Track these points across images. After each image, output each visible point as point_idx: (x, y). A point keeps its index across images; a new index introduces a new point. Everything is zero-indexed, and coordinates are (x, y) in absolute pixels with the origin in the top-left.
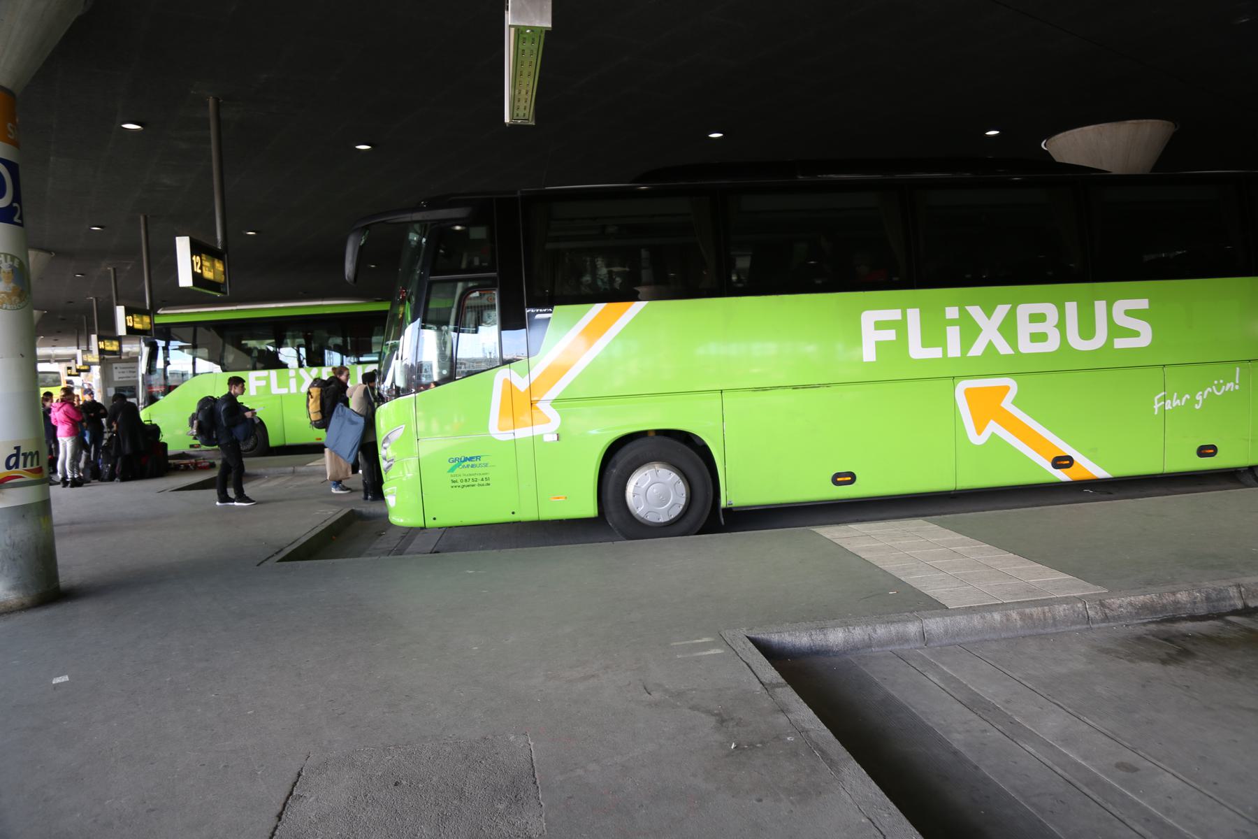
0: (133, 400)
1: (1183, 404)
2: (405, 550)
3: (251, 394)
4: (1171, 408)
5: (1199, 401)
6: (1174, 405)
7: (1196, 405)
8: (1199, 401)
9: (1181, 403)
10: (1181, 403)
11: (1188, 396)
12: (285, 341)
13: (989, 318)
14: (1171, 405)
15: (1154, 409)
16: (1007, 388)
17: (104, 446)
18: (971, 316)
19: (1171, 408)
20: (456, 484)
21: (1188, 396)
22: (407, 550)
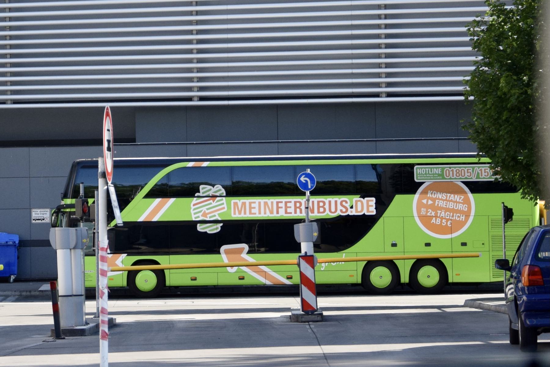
7: (322, 268)
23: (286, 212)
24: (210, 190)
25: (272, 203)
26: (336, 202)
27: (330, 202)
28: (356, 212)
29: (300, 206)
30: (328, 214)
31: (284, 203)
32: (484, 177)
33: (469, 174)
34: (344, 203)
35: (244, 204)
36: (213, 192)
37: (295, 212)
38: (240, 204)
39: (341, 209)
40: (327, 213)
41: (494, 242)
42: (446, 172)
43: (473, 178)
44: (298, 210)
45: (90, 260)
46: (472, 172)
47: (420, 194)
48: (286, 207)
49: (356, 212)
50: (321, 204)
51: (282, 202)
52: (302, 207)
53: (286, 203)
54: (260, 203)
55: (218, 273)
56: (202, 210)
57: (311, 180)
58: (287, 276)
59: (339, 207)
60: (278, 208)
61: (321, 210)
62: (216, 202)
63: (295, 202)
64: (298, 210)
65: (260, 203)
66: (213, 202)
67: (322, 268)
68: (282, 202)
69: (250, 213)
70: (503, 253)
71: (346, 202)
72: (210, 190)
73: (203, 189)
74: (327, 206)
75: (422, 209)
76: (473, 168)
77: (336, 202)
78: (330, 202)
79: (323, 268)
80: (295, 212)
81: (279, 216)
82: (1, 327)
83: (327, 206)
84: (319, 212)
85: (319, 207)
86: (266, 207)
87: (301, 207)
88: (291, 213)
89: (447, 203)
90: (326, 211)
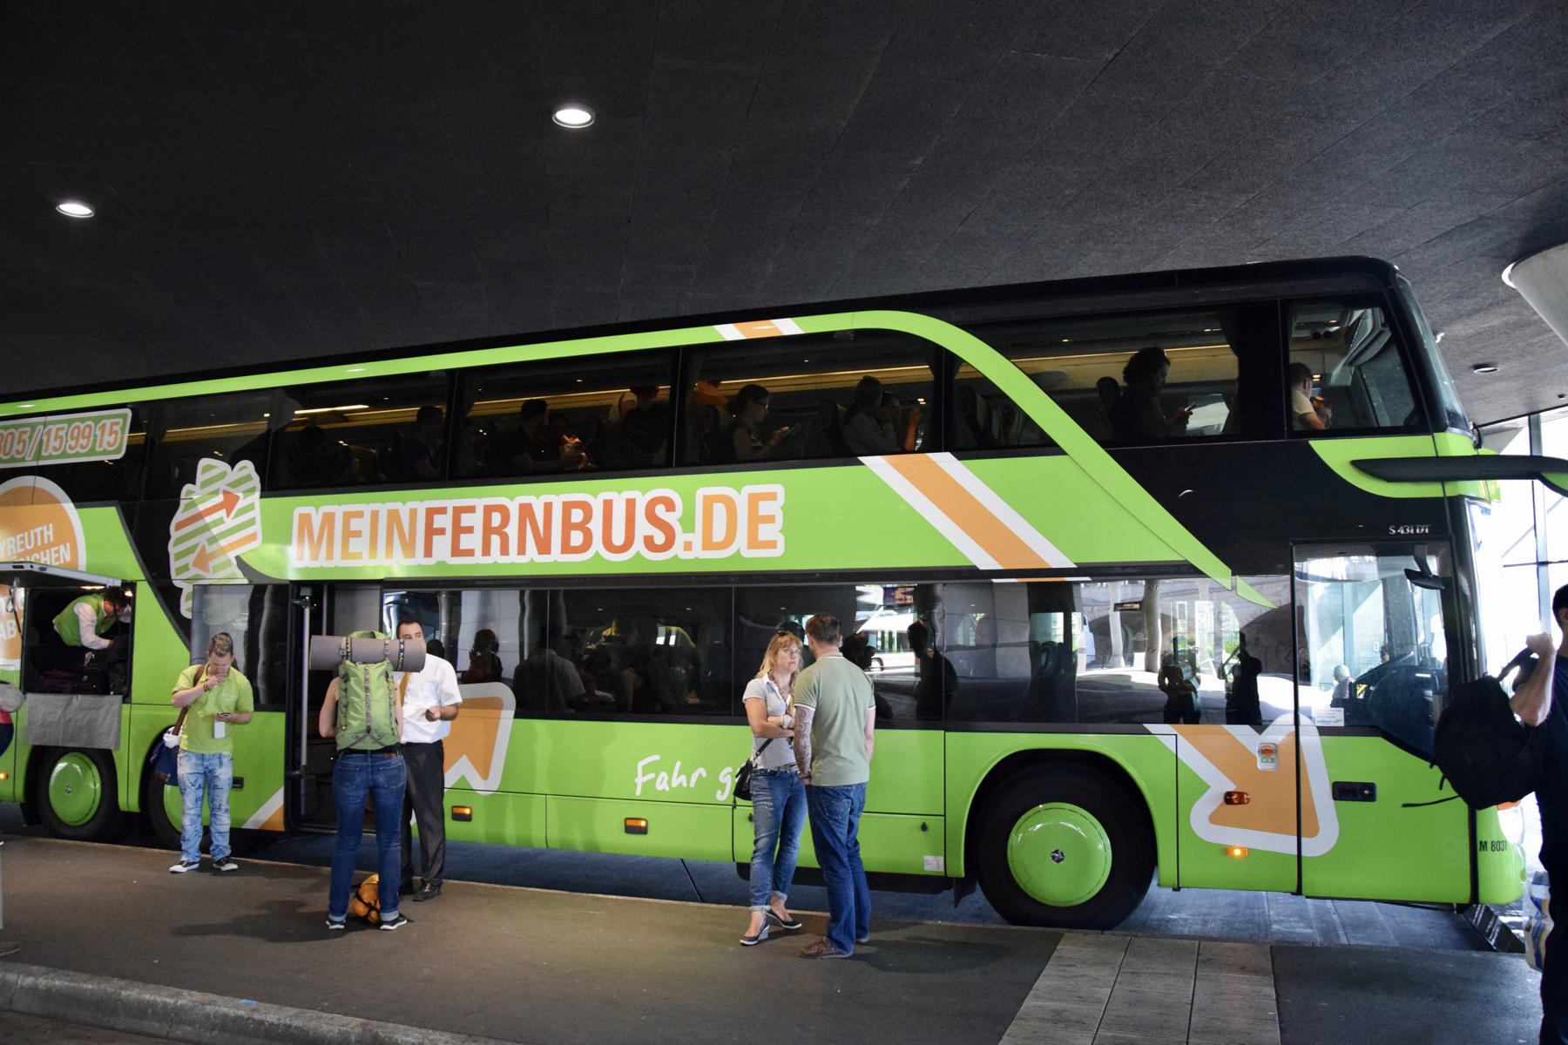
0: (1536, 317)
1: (692, 785)
2: (1015, 1015)
3: (1296, 429)
4: (667, 789)
5: (725, 784)
6: (674, 785)
7: (719, 792)
8: (725, 784)
9: (688, 782)
10: (688, 782)
11: (702, 771)
12: (45, 988)
13: (463, 777)
14: (669, 783)
15: (636, 784)
16: (485, 776)
17: (698, 697)
18: (507, 756)
19: (667, 789)
20: (224, 795)
21: (702, 771)
22: (1018, 1014)
23: (456, 551)
24: (224, 474)
25: (413, 512)
26: (631, 504)
27: (608, 505)
28: (705, 548)
29: (500, 525)
30: (600, 556)
31: (450, 512)
32: (105, 450)
33: (20, 447)
34: (660, 510)
35: (329, 519)
36: (228, 485)
37: (486, 551)
38: (317, 522)
39: (648, 533)
40: (638, 553)
42: (73, 429)
43: (27, 458)
44: (495, 540)
45: (126, 707)
46: (27, 441)
47: (59, 503)
48: (458, 530)
49: (705, 548)
50: (577, 516)
51: (471, 509)
52: (509, 526)
53: (458, 511)
54: (375, 514)
55: (943, 818)
56: (198, 544)
57: (115, 450)
58: (626, 819)
59: (643, 528)
60: (431, 532)
61: (577, 538)
62: (236, 516)
63: (489, 510)
64: (495, 540)
65: (375, 514)
66: (228, 515)
67: (719, 792)
68: (471, 509)
69: (754, 543)
70: (133, 712)
71: (670, 506)
72: (224, 474)
73: (208, 468)
74: (596, 525)
75: (660, 641)
76: (33, 427)
77: (631, 504)
78: (608, 505)
79: (722, 794)
80: (486, 551)
81: (433, 563)
82: (1563, 242)
83: (596, 525)
84: (567, 548)
85: (568, 526)
86: (304, 529)
87: (505, 527)
88: (470, 553)
89: (22, 539)
90: (593, 546)
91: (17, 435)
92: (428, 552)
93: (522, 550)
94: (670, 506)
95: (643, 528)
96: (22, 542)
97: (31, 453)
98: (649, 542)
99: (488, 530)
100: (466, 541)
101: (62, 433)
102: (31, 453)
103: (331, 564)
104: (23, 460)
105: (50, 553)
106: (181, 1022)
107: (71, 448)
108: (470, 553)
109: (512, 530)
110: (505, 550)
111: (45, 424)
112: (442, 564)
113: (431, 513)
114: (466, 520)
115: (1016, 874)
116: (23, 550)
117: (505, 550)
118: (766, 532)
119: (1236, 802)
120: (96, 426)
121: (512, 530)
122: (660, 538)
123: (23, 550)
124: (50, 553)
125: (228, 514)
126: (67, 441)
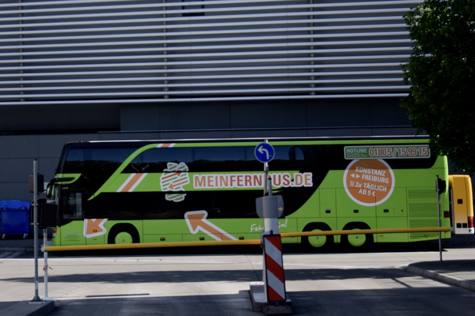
0: (32, 224)
23: (239, 185)
26: (280, 176)
34: (286, 177)
35: (204, 178)
37: (246, 185)
41: (425, 221)
43: (393, 156)
44: (248, 183)
48: (239, 180)
54: (216, 177)
59: (282, 181)
60: (232, 181)
63: (246, 177)
64: (248, 183)
65: (216, 177)
71: (288, 176)
73: (170, 165)
77: (280, 176)
80: (246, 185)
88: (242, 185)
91: (387, 150)
92: (231, 185)
93: (255, 185)
94: (288, 176)
95: (282, 181)
96: (364, 177)
97: (394, 154)
98: (284, 184)
99: (246, 181)
100: (241, 183)
101: (405, 150)
102: (394, 154)
103: (222, 187)
104: (392, 157)
105: (381, 179)
106: (126, 301)
107: (409, 154)
108: (242, 185)
109: (252, 180)
110: (251, 185)
111: (407, 148)
112: (235, 188)
113: (231, 177)
114: (240, 178)
115: (316, 246)
116: (370, 180)
117: (251, 185)
118: (211, 183)
119: (263, 229)
120: (417, 149)
121: (252, 180)
122: (286, 183)
123: (370, 180)
124: (381, 179)
125: (179, 176)
126: (407, 152)
